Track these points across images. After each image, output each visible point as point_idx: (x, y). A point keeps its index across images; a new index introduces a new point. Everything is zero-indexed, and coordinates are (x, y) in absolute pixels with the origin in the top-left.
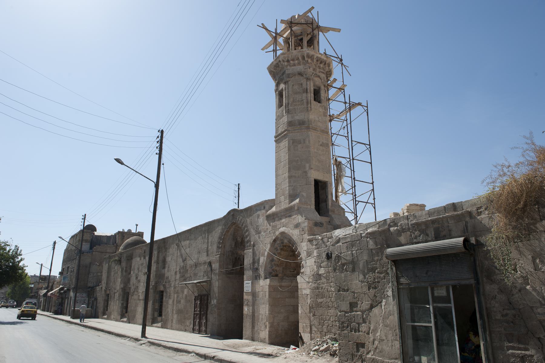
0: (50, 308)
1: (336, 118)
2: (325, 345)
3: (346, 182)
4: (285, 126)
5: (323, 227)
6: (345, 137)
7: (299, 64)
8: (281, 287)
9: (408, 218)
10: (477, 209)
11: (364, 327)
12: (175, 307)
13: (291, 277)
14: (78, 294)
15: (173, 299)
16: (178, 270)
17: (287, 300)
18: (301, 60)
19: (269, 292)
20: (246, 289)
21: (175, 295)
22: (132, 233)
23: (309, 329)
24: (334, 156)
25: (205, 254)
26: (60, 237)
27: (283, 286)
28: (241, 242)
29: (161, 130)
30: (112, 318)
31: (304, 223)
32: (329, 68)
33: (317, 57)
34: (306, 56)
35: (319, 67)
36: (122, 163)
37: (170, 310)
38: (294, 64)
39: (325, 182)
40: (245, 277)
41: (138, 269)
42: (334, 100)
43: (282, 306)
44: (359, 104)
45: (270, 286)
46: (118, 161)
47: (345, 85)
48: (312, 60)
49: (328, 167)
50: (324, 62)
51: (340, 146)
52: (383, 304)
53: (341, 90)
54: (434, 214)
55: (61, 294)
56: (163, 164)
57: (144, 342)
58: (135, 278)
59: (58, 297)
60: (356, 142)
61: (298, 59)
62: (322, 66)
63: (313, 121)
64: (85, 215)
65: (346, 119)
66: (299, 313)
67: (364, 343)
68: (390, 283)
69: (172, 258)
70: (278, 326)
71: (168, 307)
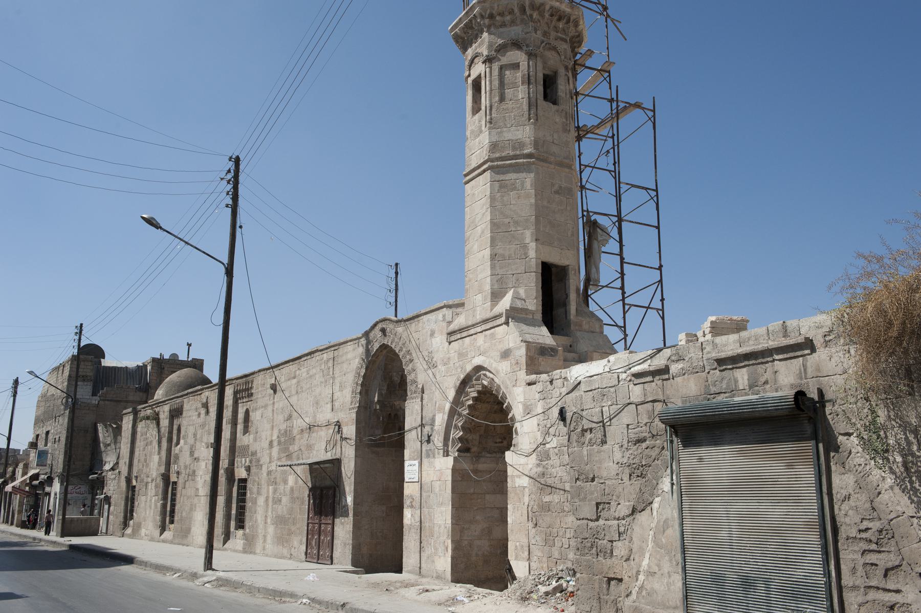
0: (10, 516)
1: (592, 133)
2: (554, 583)
3: (607, 268)
4: (485, 152)
5: (557, 358)
6: (610, 171)
7: (513, 22)
8: (476, 471)
9: (704, 346)
10: (825, 336)
11: (620, 549)
12: (270, 510)
13: (496, 452)
14: (70, 488)
15: (266, 496)
16: (275, 437)
17: (488, 497)
18: (518, 14)
19: (453, 481)
20: (409, 476)
21: (271, 487)
22: (180, 362)
23: (526, 553)
24: (585, 211)
25: (329, 406)
26: (31, 373)
27: (481, 471)
28: (400, 382)
29: (234, 157)
30: (143, 534)
31: (519, 348)
32: (575, 29)
33: (552, 7)
34: (529, 6)
35: (556, 29)
36: (157, 226)
37: (259, 517)
38: (504, 22)
39: (565, 267)
40: (407, 453)
41: (195, 435)
42: (588, 95)
43: (477, 509)
44: (638, 105)
45: (454, 470)
46: (150, 222)
47: (611, 63)
48: (542, 15)
49: (569, 236)
50: (566, 17)
51: (598, 192)
52: (655, 505)
53: (602, 73)
54: (748, 342)
55: (33, 487)
56: (241, 227)
57: (210, 580)
58: (189, 453)
59: (27, 494)
60: (627, 184)
61: (511, 12)
62: (561, 26)
63: (542, 142)
64: (81, 325)
65: (610, 135)
66: (509, 523)
67: (620, 578)
68: (667, 468)
69: (262, 414)
70: (470, 546)
71: (255, 512)
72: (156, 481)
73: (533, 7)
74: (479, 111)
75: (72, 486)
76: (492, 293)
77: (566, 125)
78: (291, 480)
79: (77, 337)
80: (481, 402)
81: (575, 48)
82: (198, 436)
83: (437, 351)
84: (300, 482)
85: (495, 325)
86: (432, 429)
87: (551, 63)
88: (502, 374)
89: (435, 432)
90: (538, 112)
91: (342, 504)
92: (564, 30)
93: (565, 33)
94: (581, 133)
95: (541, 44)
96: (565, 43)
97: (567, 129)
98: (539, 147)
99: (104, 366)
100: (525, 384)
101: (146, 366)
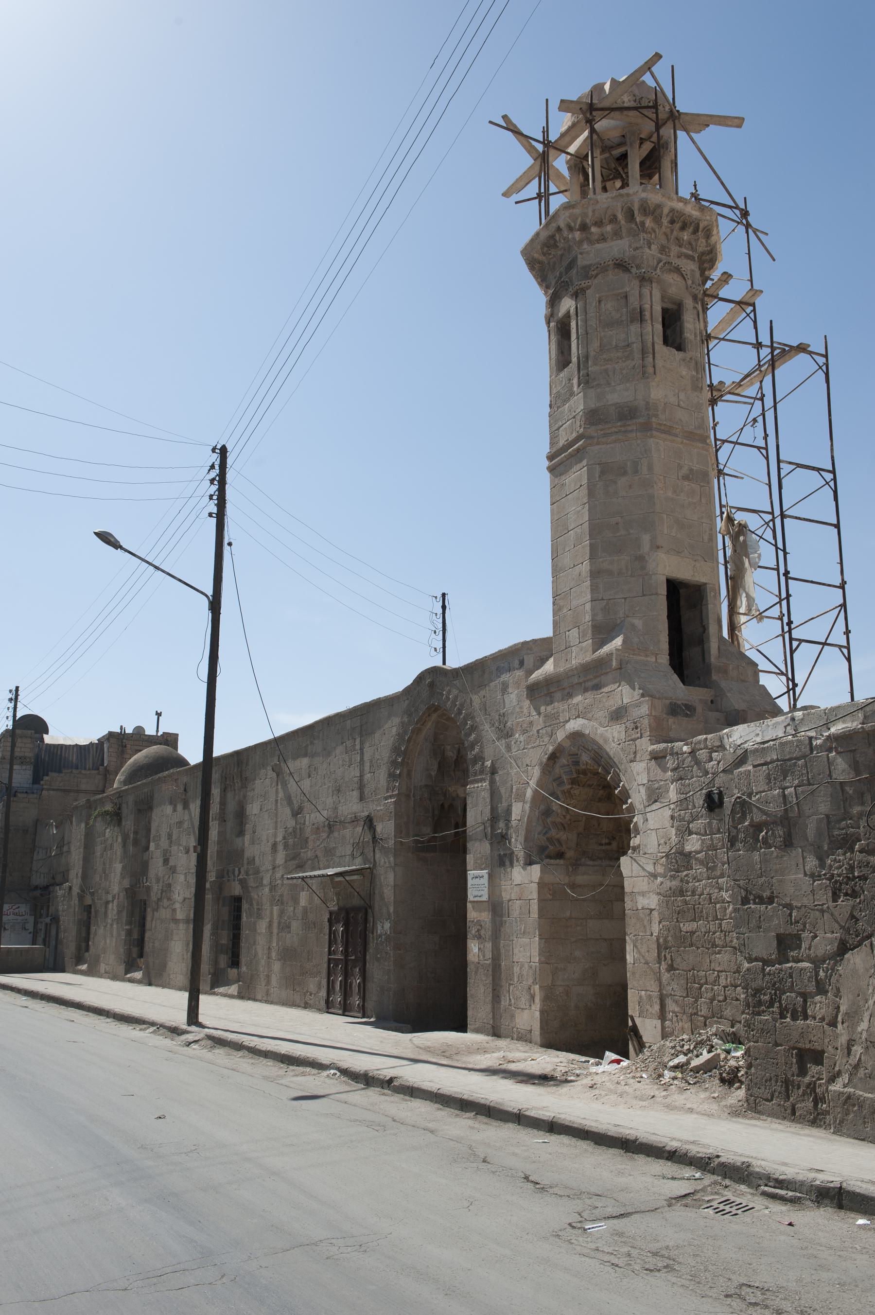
2: (705, 1052)
6: (759, 448)
7: (617, 234)
8: (573, 886)
11: (819, 1006)
13: (601, 859)
16: (279, 838)
18: (623, 222)
19: (541, 900)
20: (476, 893)
22: (147, 738)
23: (657, 1007)
24: (724, 506)
25: (356, 794)
27: (580, 886)
29: (219, 447)
30: (103, 971)
31: (638, 705)
32: (707, 241)
33: (672, 210)
34: (639, 210)
35: (679, 242)
36: (116, 545)
38: (603, 235)
40: (470, 859)
41: (170, 836)
42: (723, 339)
44: (802, 348)
45: (541, 885)
46: (105, 538)
47: (757, 291)
48: (657, 220)
49: (706, 540)
50: (693, 224)
51: (743, 478)
53: (743, 306)
56: (230, 544)
57: (196, 1038)
60: (790, 463)
61: (614, 220)
62: (685, 238)
64: (17, 688)
67: (820, 1049)
71: (255, 942)
72: (118, 899)
73: (645, 211)
74: (568, 365)
75: (9, 905)
76: (594, 627)
77: (697, 380)
78: (304, 898)
79: (12, 705)
80: (579, 785)
81: (705, 271)
82: (174, 837)
83: (512, 713)
84: (317, 901)
86: (507, 825)
87: (673, 291)
88: (613, 744)
89: (511, 831)
90: (656, 361)
91: (377, 932)
92: (690, 244)
93: (692, 248)
94: (716, 394)
95: (658, 263)
96: (691, 262)
97: (698, 387)
98: (659, 413)
99: (47, 744)
101: (103, 743)
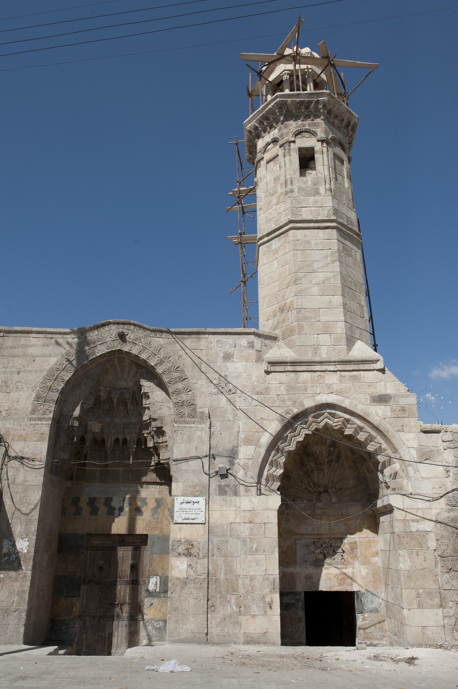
85: (362, 368)
100: (420, 431)
